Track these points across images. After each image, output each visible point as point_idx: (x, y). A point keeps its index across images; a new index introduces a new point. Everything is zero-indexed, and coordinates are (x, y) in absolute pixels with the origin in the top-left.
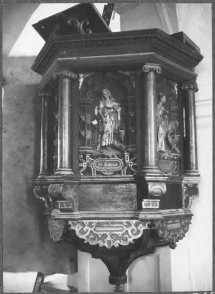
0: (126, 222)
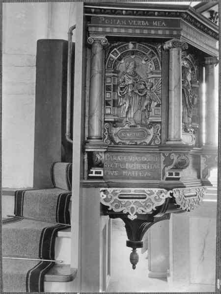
0: (149, 191)
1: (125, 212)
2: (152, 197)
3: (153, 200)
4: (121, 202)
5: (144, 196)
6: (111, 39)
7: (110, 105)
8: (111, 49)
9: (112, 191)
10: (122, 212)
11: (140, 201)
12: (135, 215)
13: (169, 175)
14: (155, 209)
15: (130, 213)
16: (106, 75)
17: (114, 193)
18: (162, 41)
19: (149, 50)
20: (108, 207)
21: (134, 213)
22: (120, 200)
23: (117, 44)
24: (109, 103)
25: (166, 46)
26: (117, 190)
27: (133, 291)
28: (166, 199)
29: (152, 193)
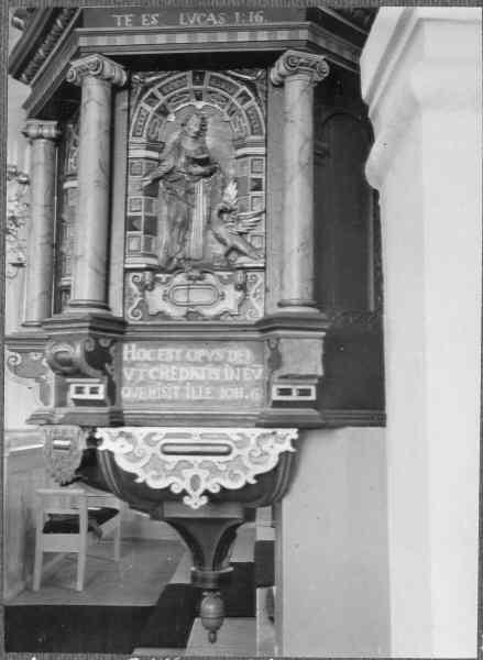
0: (239, 434)
1: (176, 490)
2: (245, 452)
3: (246, 462)
4: (165, 462)
5: (225, 449)
6: (132, 63)
7: (136, 229)
8: (146, 89)
9: (145, 435)
10: (168, 489)
11: (215, 459)
12: (201, 495)
13: (300, 395)
14: (253, 482)
15: (191, 492)
16: (262, 150)
17: (148, 440)
18: (265, 60)
19: (238, 88)
20: (134, 476)
21: (200, 491)
22: (163, 457)
23: (58, 73)
24: (135, 224)
25: (274, 75)
26: (154, 434)
27: (437, 657)
28: (281, 455)
29: (242, 443)
